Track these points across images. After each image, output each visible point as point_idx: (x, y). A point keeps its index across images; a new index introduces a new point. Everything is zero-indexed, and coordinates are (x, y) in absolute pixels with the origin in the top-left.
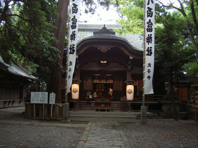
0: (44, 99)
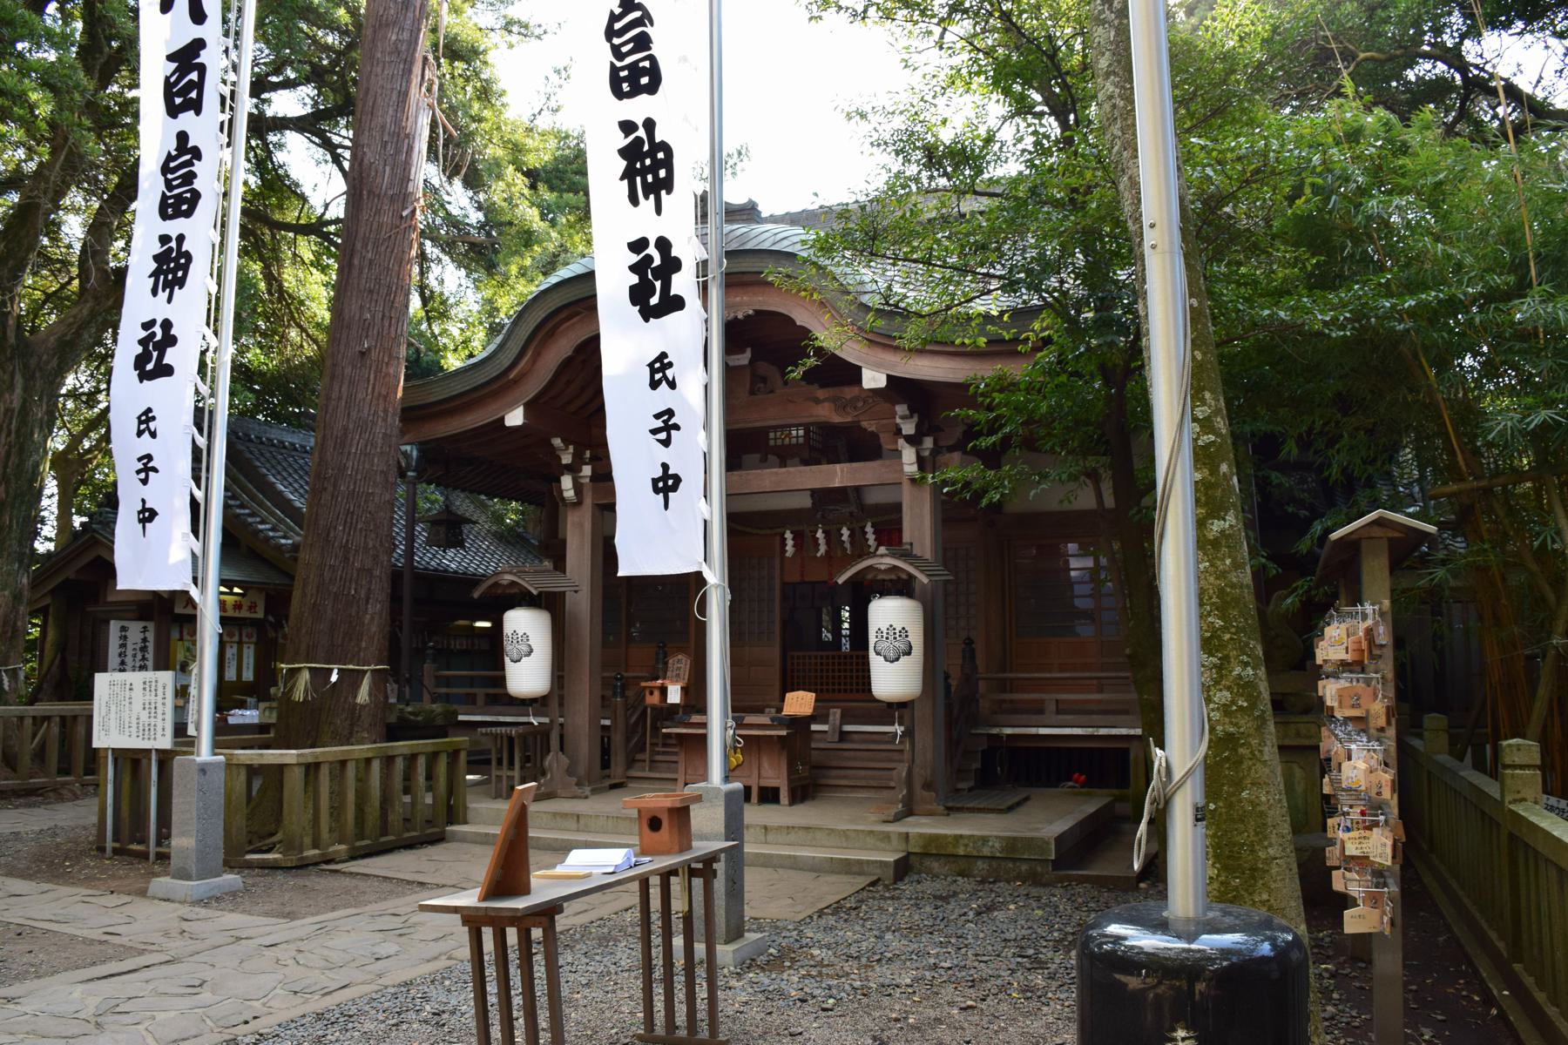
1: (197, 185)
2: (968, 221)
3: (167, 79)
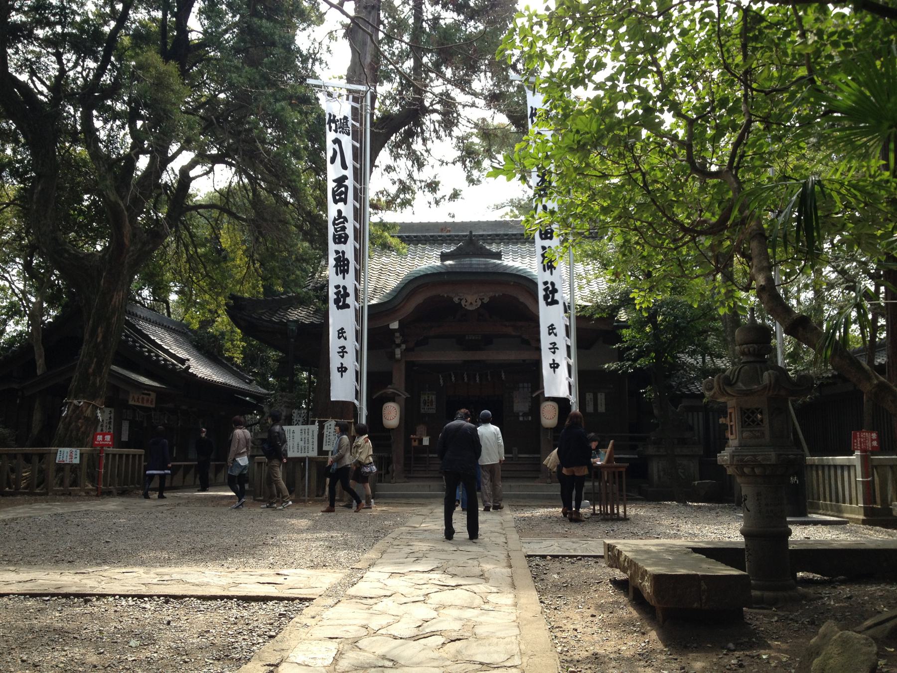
0: (306, 445)
1: (347, 231)
2: (137, 292)
3: (333, 189)
